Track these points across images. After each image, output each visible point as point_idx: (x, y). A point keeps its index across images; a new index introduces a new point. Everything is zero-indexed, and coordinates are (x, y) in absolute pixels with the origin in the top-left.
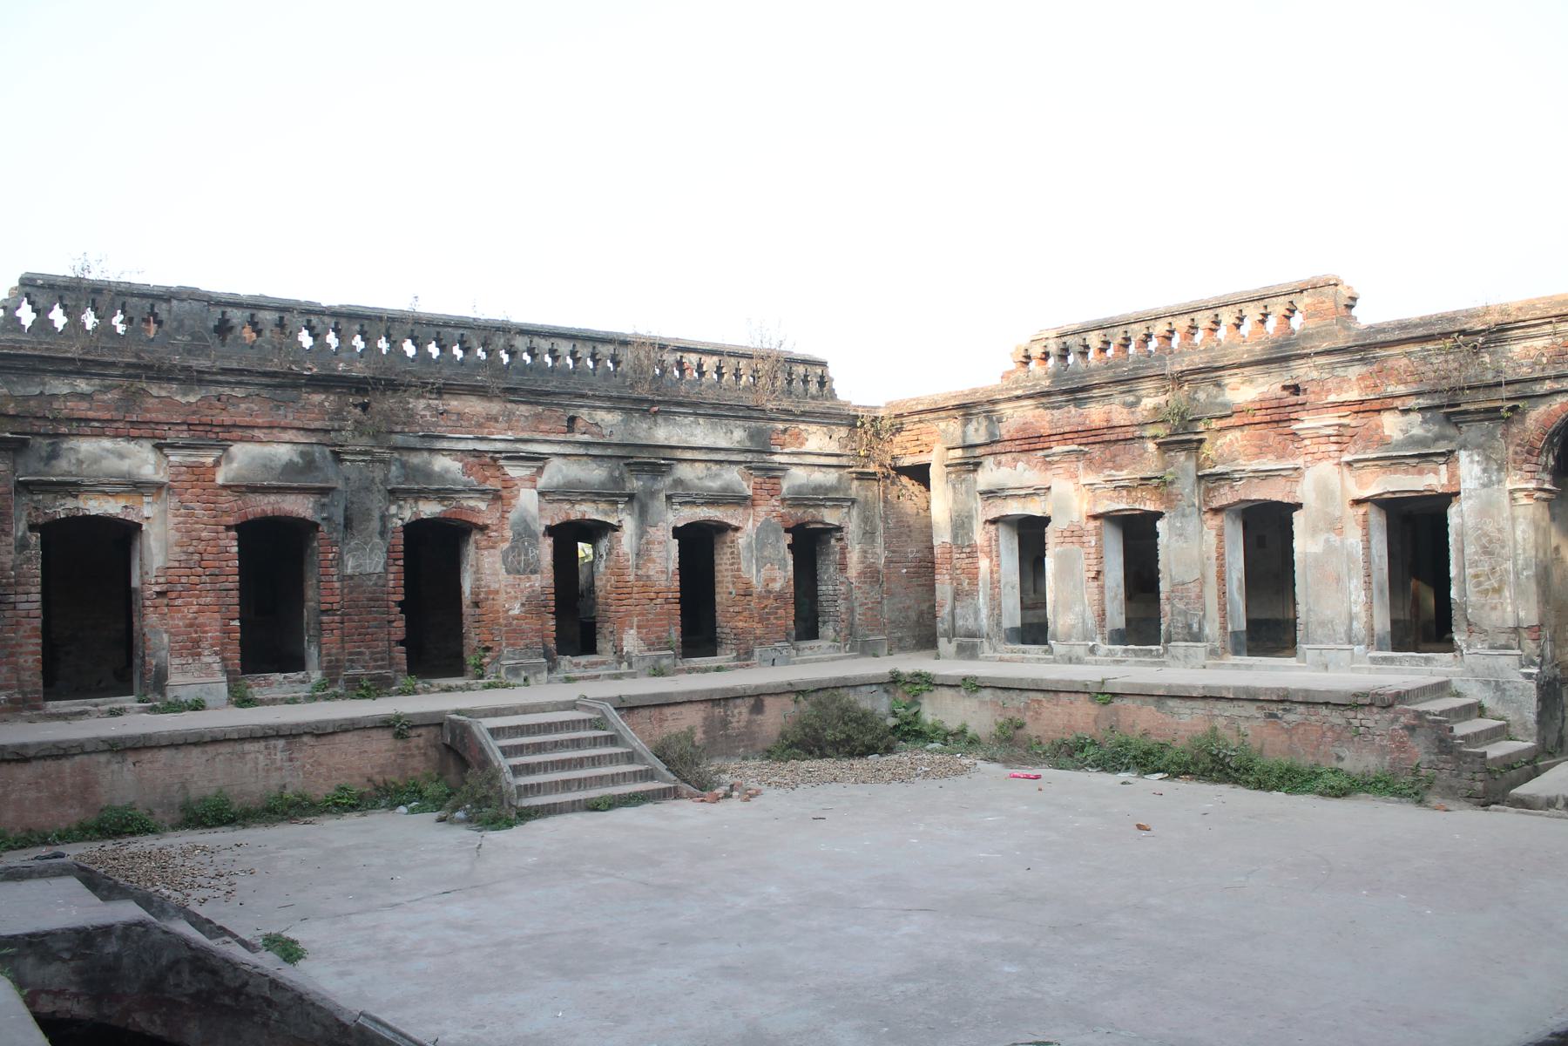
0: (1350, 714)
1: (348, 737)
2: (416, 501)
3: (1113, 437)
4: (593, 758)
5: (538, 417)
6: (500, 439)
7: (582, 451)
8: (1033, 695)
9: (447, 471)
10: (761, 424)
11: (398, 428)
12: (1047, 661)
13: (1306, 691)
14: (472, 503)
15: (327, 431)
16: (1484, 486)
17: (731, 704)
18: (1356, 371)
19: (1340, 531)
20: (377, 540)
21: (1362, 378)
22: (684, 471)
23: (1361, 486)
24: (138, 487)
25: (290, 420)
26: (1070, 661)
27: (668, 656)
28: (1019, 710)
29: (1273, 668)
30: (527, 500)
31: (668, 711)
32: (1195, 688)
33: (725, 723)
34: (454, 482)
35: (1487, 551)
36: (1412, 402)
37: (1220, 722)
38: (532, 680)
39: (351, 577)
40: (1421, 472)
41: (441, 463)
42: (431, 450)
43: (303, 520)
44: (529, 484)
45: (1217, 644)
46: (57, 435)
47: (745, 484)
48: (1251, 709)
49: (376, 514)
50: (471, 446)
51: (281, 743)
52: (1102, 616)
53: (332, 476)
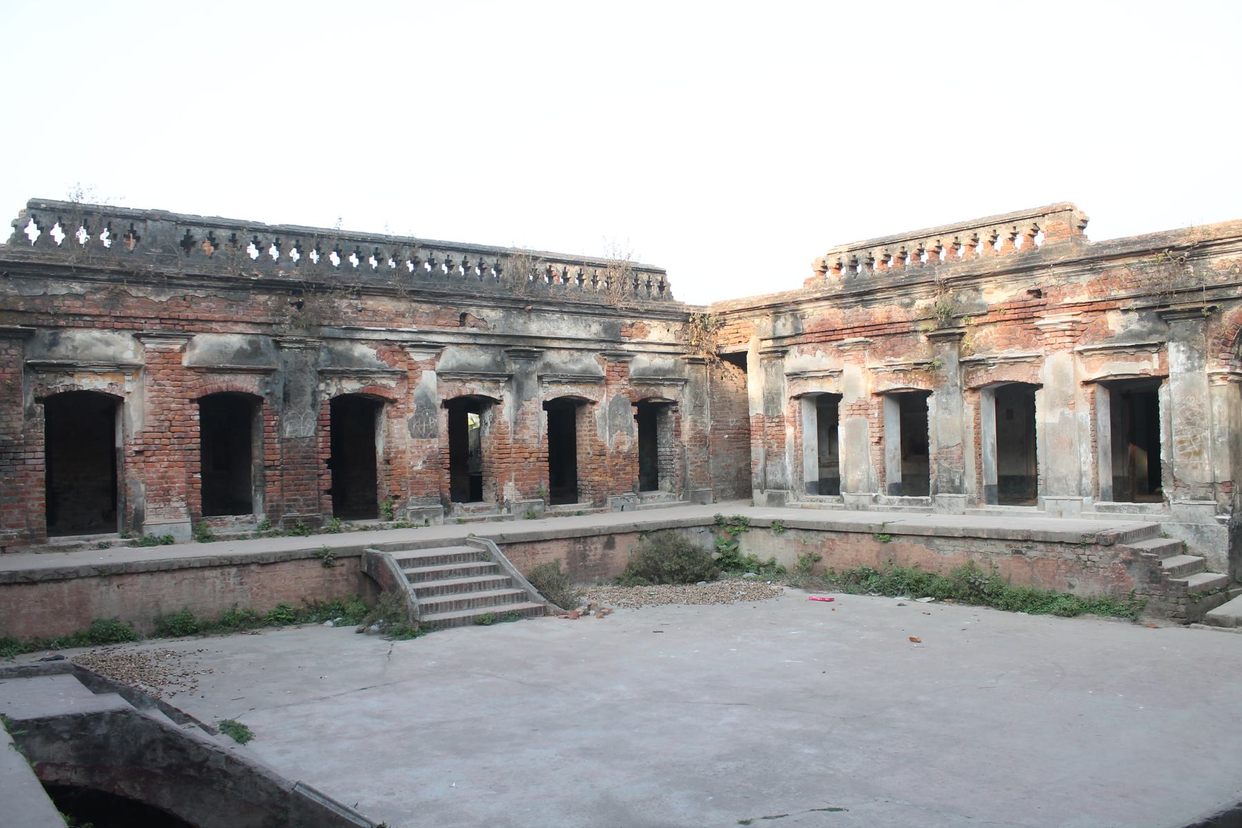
0: (1080, 551)
1: (286, 566)
2: (340, 379)
3: (892, 331)
4: (480, 583)
5: (436, 313)
6: (406, 331)
7: (471, 341)
8: (828, 535)
9: (364, 356)
10: (613, 320)
11: (326, 322)
12: (839, 508)
13: (1045, 533)
14: (384, 382)
15: (270, 325)
16: (1188, 370)
17: (589, 541)
18: (1086, 279)
19: (1072, 406)
20: (309, 410)
21: (1091, 284)
22: (552, 357)
23: (1089, 370)
24: (121, 368)
25: (240, 315)
26: (858, 508)
27: (539, 503)
28: (816, 547)
29: (1019, 514)
30: (428, 379)
31: (539, 547)
32: (957, 530)
33: (584, 556)
34: (370, 365)
35: (1190, 422)
36: (1131, 304)
37: (976, 557)
38: (431, 522)
39: (289, 440)
40: (1137, 360)
41: (360, 350)
42: (352, 340)
43: (251, 395)
44: (429, 367)
45: (975, 495)
46: (57, 327)
47: (600, 367)
48: (1002, 547)
49: (309, 390)
50: (384, 336)
51: (234, 570)
52: (883, 472)
53: (274, 360)
